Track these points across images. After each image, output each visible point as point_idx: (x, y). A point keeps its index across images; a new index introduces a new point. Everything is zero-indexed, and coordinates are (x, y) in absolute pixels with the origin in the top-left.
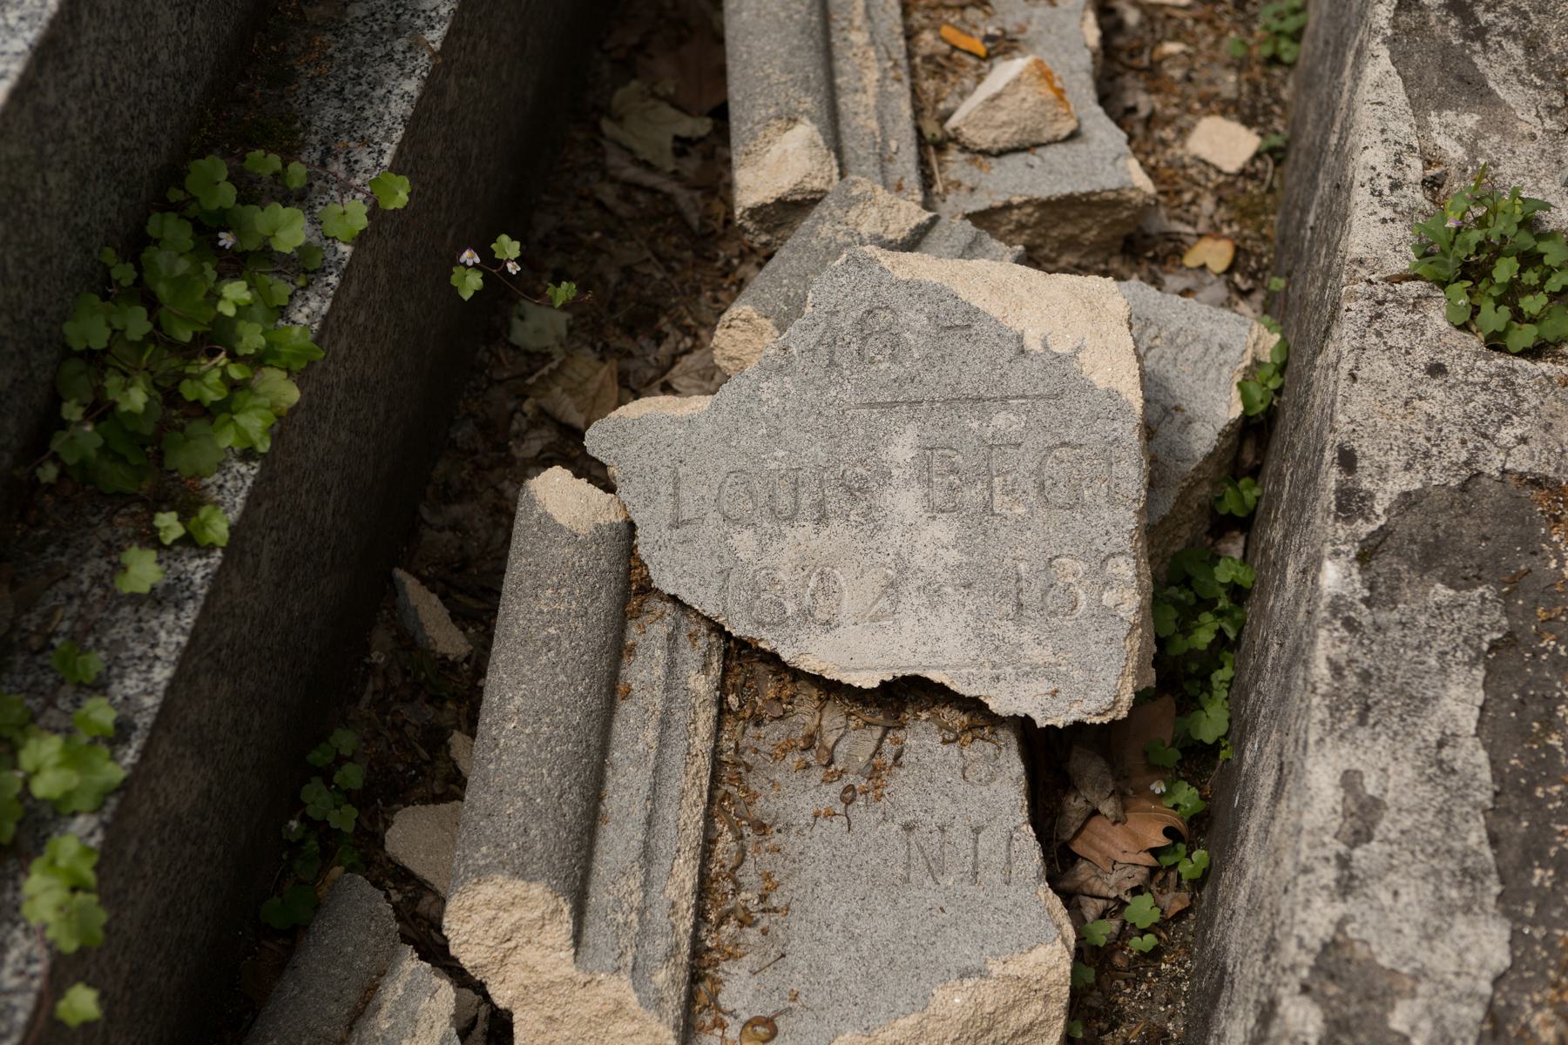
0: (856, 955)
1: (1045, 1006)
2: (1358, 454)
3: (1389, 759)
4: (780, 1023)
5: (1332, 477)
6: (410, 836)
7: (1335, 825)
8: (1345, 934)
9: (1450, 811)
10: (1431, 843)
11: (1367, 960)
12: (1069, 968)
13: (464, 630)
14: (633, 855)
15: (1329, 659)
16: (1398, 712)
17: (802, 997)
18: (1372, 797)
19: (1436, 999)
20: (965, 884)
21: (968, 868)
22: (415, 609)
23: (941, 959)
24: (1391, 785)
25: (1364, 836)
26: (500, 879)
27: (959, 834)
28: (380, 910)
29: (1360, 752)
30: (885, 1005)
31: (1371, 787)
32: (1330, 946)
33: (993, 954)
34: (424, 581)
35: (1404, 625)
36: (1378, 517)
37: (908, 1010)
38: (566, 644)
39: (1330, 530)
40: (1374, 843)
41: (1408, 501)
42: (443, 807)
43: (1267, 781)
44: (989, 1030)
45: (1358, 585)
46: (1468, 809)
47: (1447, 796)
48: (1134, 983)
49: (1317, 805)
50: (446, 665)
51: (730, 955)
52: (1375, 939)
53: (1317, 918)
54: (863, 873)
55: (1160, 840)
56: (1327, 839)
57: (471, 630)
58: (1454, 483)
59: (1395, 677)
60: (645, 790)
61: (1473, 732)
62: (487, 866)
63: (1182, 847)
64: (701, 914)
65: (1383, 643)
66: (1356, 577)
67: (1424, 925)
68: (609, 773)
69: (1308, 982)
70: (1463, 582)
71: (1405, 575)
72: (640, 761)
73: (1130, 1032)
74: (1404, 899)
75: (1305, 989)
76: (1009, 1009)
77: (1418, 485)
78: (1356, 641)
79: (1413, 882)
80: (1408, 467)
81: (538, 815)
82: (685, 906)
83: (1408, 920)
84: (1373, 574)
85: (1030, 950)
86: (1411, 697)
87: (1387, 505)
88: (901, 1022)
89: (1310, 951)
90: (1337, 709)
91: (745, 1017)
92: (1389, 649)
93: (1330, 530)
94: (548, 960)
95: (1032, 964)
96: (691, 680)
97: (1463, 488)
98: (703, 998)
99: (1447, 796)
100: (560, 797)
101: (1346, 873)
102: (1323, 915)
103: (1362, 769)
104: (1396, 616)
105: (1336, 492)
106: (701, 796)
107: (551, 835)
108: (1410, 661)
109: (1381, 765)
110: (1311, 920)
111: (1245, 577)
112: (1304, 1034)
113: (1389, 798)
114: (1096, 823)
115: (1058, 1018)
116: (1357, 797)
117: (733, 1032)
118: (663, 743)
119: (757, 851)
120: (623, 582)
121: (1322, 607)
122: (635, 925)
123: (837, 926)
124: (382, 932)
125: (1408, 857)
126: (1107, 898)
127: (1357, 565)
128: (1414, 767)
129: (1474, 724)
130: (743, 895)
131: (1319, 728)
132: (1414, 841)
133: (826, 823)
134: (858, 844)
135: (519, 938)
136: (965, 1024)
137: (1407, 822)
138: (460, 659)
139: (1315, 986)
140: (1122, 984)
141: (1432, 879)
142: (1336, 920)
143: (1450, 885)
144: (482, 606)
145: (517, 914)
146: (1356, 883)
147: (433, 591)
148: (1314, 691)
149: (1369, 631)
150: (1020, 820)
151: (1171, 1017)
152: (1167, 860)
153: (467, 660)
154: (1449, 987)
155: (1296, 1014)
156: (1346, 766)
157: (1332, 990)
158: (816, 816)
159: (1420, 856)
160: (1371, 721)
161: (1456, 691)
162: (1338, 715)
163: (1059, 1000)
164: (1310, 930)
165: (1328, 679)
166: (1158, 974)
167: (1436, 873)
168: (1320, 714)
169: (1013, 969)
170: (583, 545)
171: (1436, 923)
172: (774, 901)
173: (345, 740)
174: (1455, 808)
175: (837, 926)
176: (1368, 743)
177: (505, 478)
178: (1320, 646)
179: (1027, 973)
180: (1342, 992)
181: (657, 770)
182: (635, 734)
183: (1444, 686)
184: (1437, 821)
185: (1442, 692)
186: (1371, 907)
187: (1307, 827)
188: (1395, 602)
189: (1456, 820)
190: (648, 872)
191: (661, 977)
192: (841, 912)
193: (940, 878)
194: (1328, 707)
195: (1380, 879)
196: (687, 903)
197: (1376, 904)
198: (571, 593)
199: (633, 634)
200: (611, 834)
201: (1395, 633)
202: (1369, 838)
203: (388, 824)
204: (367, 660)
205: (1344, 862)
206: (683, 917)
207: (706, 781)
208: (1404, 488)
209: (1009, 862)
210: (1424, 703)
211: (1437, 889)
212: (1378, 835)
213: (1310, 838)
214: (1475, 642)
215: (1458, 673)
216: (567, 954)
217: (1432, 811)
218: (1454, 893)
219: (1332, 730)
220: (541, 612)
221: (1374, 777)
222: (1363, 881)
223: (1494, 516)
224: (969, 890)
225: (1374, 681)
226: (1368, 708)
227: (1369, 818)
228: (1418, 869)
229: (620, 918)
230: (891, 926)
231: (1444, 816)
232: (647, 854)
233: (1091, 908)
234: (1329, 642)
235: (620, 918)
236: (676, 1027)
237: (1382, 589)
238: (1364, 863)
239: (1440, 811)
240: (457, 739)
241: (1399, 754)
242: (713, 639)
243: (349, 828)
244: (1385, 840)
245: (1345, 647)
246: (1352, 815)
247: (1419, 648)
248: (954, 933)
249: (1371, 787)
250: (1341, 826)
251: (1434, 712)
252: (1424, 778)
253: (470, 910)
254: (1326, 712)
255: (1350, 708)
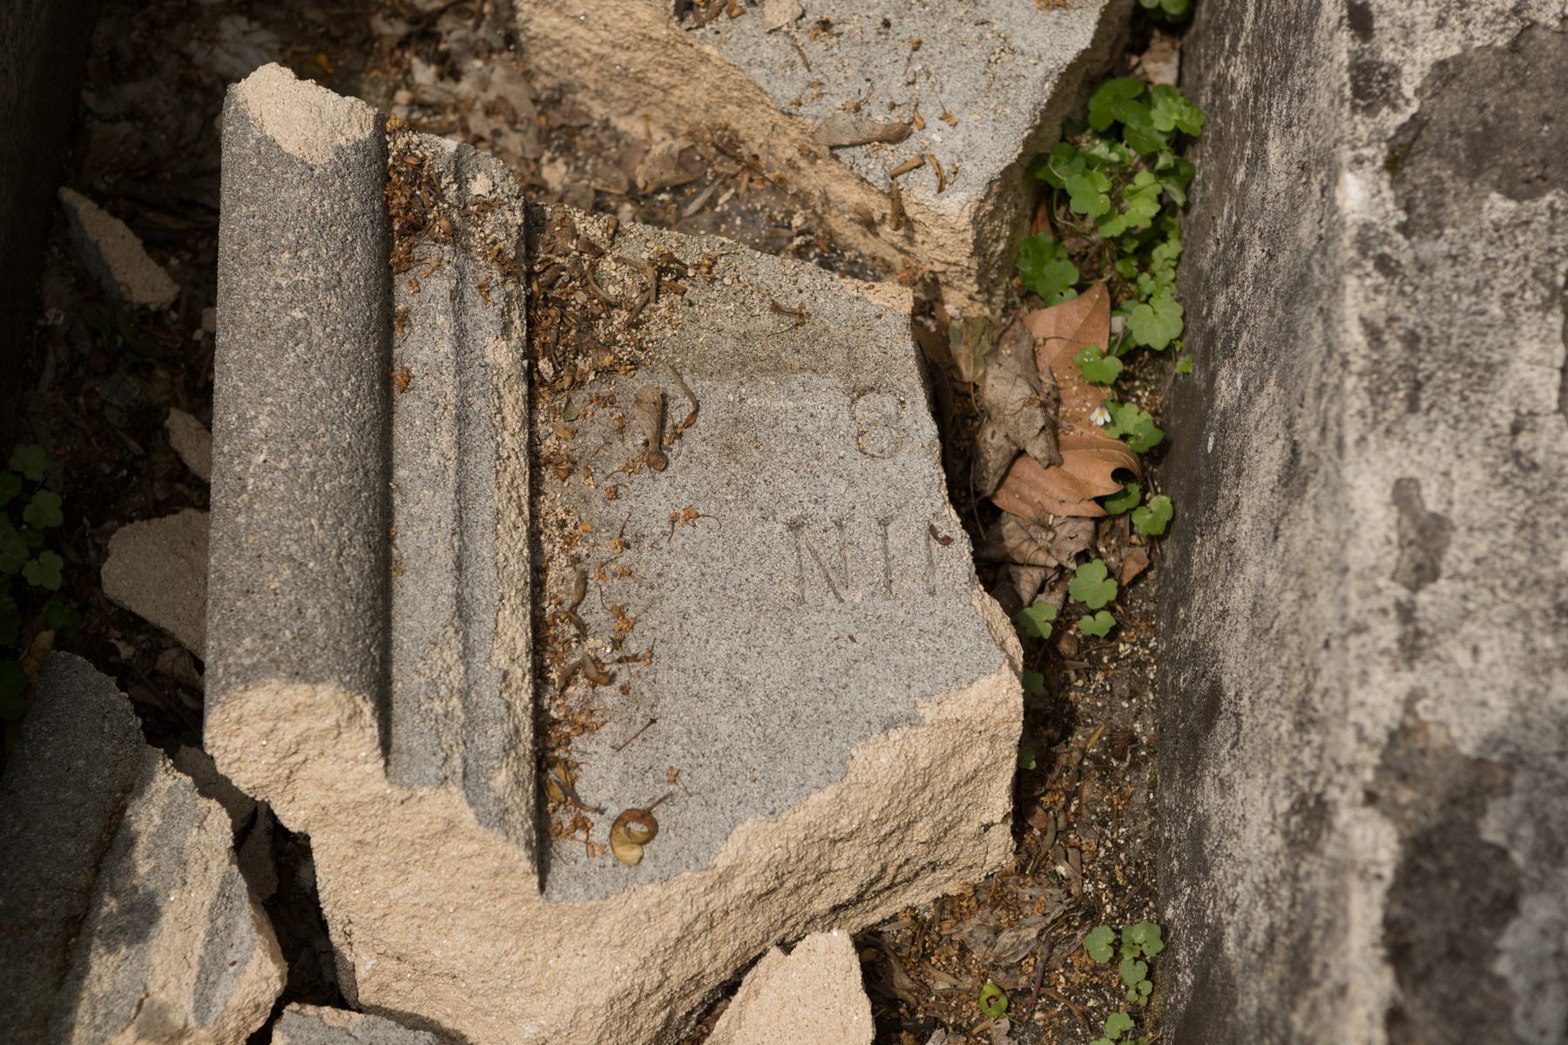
0: (748, 712)
1: (992, 747)
2: (1374, 9)
3: (1452, 457)
4: (659, 814)
5: (1343, 46)
6: (133, 568)
7: (1391, 560)
8: (1415, 715)
9: (1535, 525)
10: (1514, 573)
11: (1447, 749)
12: (1020, 700)
13: (163, 262)
14: (446, 615)
15: (1362, 319)
16: (1456, 387)
17: (684, 777)
18: (1434, 516)
19: (1536, 793)
20: (878, 600)
21: (879, 576)
22: (96, 245)
23: (858, 708)
24: (1456, 494)
25: (1428, 572)
26: (275, 684)
27: (862, 530)
28: (112, 703)
29: (1413, 451)
30: (792, 778)
31: (1432, 501)
32: (1399, 735)
33: (923, 694)
34: (100, 199)
35: (1454, 258)
36: (1408, 102)
37: (823, 782)
38: (318, 331)
39: (1346, 126)
40: (1442, 582)
41: (1444, 73)
42: (171, 520)
43: (1267, 459)
44: (924, 788)
45: (1390, 206)
46: (1556, 518)
47: (1529, 502)
48: (1087, 674)
49: (1365, 534)
50: (149, 318)
51: (584, 727)
52: (1455, 719)
53: (1380, 698)
54: (743, 596)
55: (1106, 486)
56: (1382, 582)
57: (174, 262)
58: (1502, 41)
59: (1449, 337)
60: (448, 522)
61: (1554, 406)
62: (254, 667)
63: (1134, 489)
64: (539, 675)
65: (1430, 289)
66: (1388, 194)
67: (1515, 691)
68: (397, 500)
69: (1374, 788)
70: (1523, 187)
71: (1449, 185)
72: (433, 484)
73: (1088, 738)
74: (1487, 657)
75: (1371, 798)
76: (946, 760)
77: (1455, 50)
78: (1395, 289)
79: (1495, 632)
80: (1441, 23)
81: (314, 587)
82: (519, 673)
83: (1493, 687)
84: (1409, 187)
85: (970, 683)
86: (1472, 364)
87: (1418, 82)
88: (816, 798)
89: (1374, 745)
90: (1379, 392)
91: (614, 811)
92: (1438, 296)
93: (1346, 126)
94: (351, 776)
95: (973, 701)
96: (489, 351)
97: (1514, 48)
98: (556, 792)
99: (1529, 502)
100: (340, 554)
101: (1410, 628)
102: (1386, 692)
103: (1418, 475)
104: (1442, 246)
105: (1350, 69)
106: (521, 513)
107: (334, 612)
108: (1466, 312)
109: (1442, 467)
110: (1371, 700)
111: (1191, 122)
112: (1376, 863)
113: (1456, 513)
114: (1022, 467)
115: (1009, 757)
116: (1415, 518)
117: (600, 832)
118: (462, 448)
119: (603, 576)
120: (381, 224)
121: (1347, 243)
122: (459, 712)
123: (718, 674)
124: (120, 734)
125: (1486, 596)
126: (1045, 567)
127: (1387, 176)
128: (1484, 466)
129: (1555, 395)
130: (591, 642)
131: (1357, 420)
132: (1493, 572)
133: (688, 529)
134: (733, 556)
135: (310, 750)
136: (895, 789)
137: (1482, 546)
138: (166, 307)
139: (1384, 793)
140: (1073, 675)
141: (1520, 625)
142: (1402, 697)
143: (1543, 631)
144: (183, 225)
145: (302, 724)
146: (1424, 641)
147: (115, 213)
148: (1345, 364)
149: (1411, 271)
150: (939, 504)
151: (1138, 714)
152: (1117, 507)
153: (175, 306)
154: (1552, 775)
155: (1364, 838)
156: (1397, 474)
157: (1406, 796)
158: (673, 520)
159: (1502, 594)
160: (1424, 405)
161: (1529, 349)
162: (1380, 400)
163: (1009, 738)
164: (1371, 715)
165: (1364, 349)
166: (1115, 659)
167: (1524, 615)
168: (1357, 402)
169: (951, 710)
170: (322, 181)
171: (1529, 686)
172: (633, 646)
173: (31, 460)
174: (1541, 519)
175: (718, 674)
176: (1422, 437)
177: (191, 38)
178: (1349, 301)
179: (968, 713)
180: (1417, 796)
181: (460, 490)
182: (424, 441)
183: (1513, 344)
184: (1520, 541)
185: (1510, 352)
186: (1446, 674)
187: (1355, 568)
188: (1440, 226)
189: (1544, 536)
190: (466, 637)
191: (501, 779)
192: (721, 653)
193: (843, 593)
194: (1366, 389)
195: (1454, 632)
196: (521, 673)
197: (1452, 669)
198: (316, 255)
199: (404, 296)
200: (411, 589)
201: (1444, 273)
202: (1435, 575)
203: (103, 554)
204: (41, 322)
205: (1406, 613)
206: (519, 689)
207: (524, 491)
208: (1439, 56)
209: (931, 563)
210: (1486, 373)
211: (1527, 638)
212: (1446, 570)
213: (1361, 584)
214: (1547, 275)
215: (1530, 323)
216: (375, 766)
217: (1512, 526)
218: (1549, 642)
219: (1376, 423)
220: (278, 288)
221: (1435, 486)
222: (1432, 637)
223: (1556, 85)
224: (883, 607)
225: (1423, 345)
226: (1418, 386)
227: (1432, 545)
228: (1501, 612)
229: (438, 707)
230: (788, 667)
231: (1527, 532)
232: (463, 611)
233: (1027, 583)
234: (1360, 295)
235: (438, 707)
236: (528, 844)
237: (1422, 209)
238: (1432, 612)
239: (1522, 526)
240: (179, 423)
241: (1464, 449)
242: (510, 287)
243: (54, 582)
244: (1457, 576)
245: (1382, 300)
246: (1411, 543)
247: (1476, 291)
248: (871, 670)
249: (1432, 501)
250: (1398, 561)
251: (1503, 384)
252: (1498, 480)
253: (239, 721)
254: (1364, 395)
255: (1396, 389)
